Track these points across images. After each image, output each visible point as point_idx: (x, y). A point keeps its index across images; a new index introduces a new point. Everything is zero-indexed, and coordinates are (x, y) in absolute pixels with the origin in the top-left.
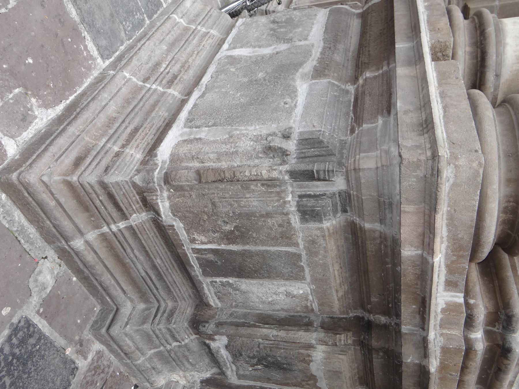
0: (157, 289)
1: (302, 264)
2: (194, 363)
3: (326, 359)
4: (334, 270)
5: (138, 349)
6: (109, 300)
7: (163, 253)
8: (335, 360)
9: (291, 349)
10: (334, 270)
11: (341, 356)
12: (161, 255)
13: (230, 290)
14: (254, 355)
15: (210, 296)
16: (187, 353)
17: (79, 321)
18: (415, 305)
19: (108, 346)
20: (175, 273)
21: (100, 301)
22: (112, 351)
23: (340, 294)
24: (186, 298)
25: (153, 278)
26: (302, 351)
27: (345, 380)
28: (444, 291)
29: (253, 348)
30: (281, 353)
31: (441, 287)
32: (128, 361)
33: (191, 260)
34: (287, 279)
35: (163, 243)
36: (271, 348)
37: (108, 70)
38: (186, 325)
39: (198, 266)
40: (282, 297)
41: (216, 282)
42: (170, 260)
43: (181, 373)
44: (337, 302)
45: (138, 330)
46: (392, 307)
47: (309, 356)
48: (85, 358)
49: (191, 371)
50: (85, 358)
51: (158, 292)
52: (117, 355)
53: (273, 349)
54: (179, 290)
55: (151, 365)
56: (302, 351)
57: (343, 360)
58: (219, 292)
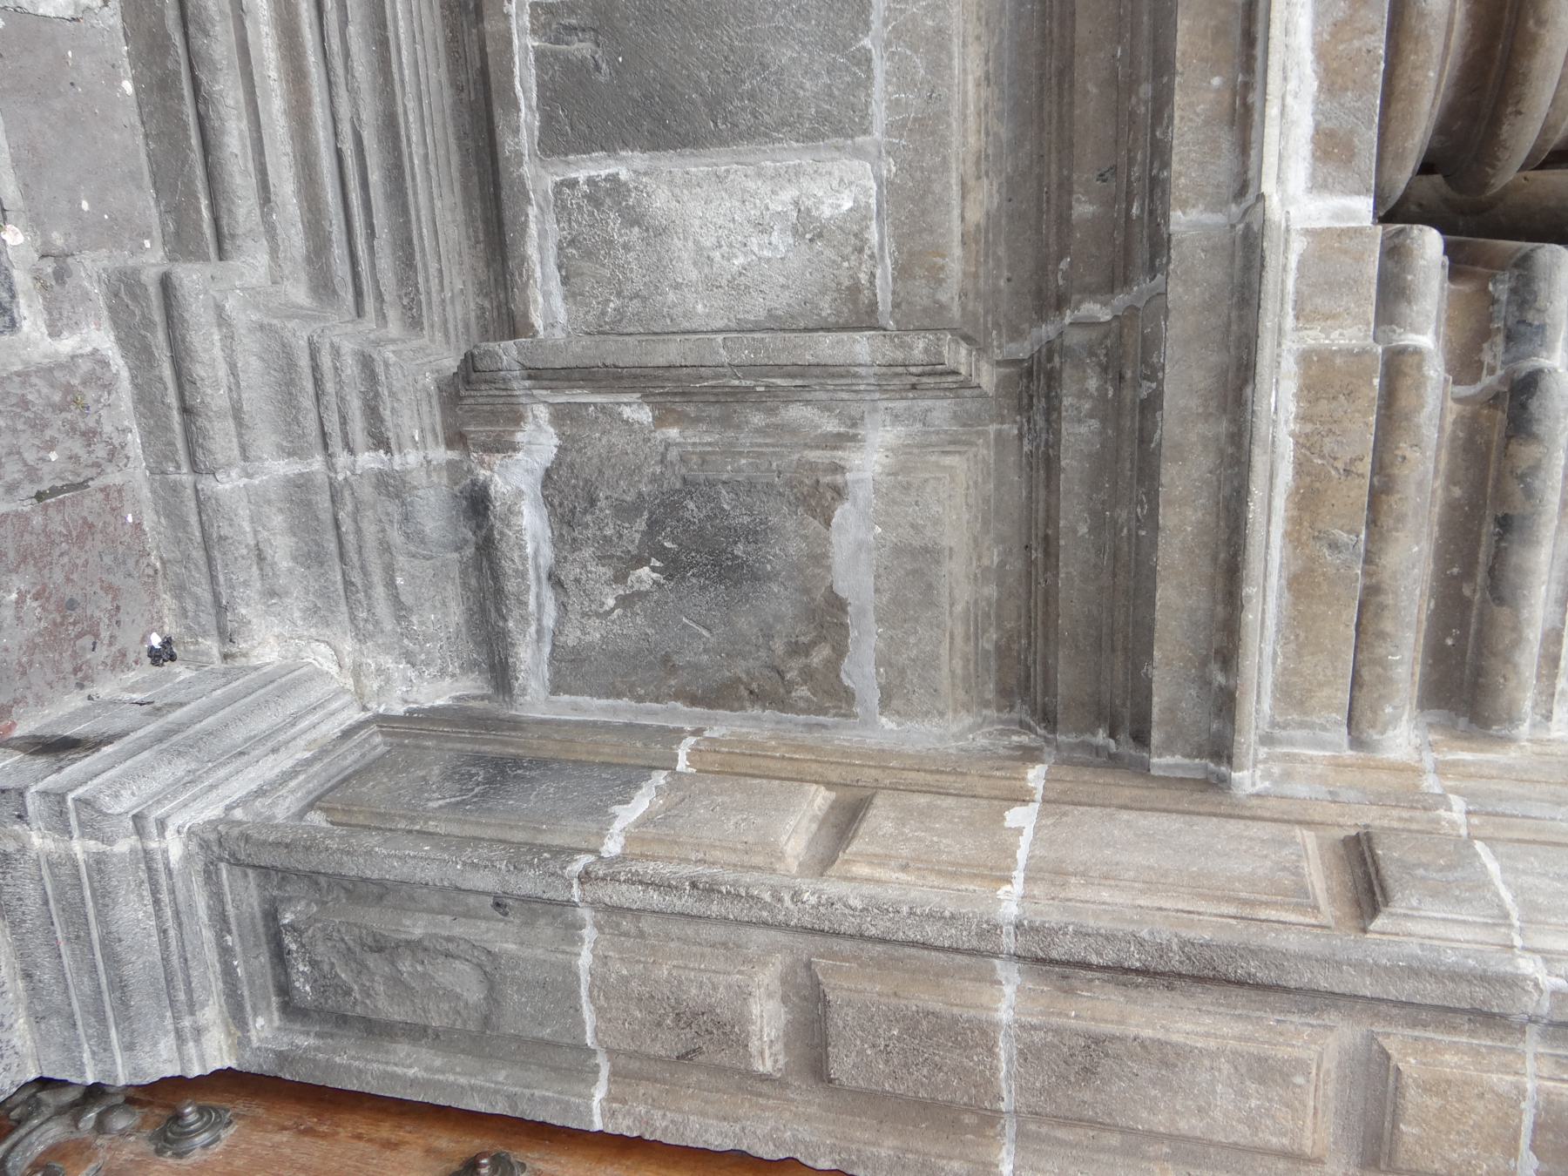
0: (371, 233)
1: (866, 42)
2: (407, 599)
3: (895, 474)
4: (965, 71)
5: (237, 413)
6: (205, 213)
7: (433, 82)
8: (927, 475)
9: (774, 453)
10: (965, 71)
11: (948, 460)
12: (423, 87)
13: (614, 222)
14: (640, 494)
15: (538, 274)
16: (396, 536)
17: (85, 205)
18: (1219, 74)
19: (139, 353)
20: (445, 190)
21: (171, 227)
22: (146, 400)
23: (975, 215)
24: (451, 326)
25: (375, 177)
26: (813, 455)
27: (949, 623)
28: (1310, 190)
29: (639, 468)
30: (739, 470)
31: (1299, 170)
32: (185, 477)
33: (517, 71)
34: (812, 136)
35: (440, 42)
36: (702, 455)
37: (327, 831)
38: (429, 380)
39: (534, 103)
40: (781, 240)
41: (573, 184)
42: (444, 124)
43: (348, 646)
44: (957, 251)
45: (262, 327)
46: (1140, 218)
47: (838, 469)
48: (55, 333)
49: (387, 649)
50: (55, 333)
51: (371, 248)
52: (154, 430)
53: (708, 458)
54: (440, 271)
55: (256, 532)
56: (813, 455)
57: (950, 469)
58: (572, 243)
